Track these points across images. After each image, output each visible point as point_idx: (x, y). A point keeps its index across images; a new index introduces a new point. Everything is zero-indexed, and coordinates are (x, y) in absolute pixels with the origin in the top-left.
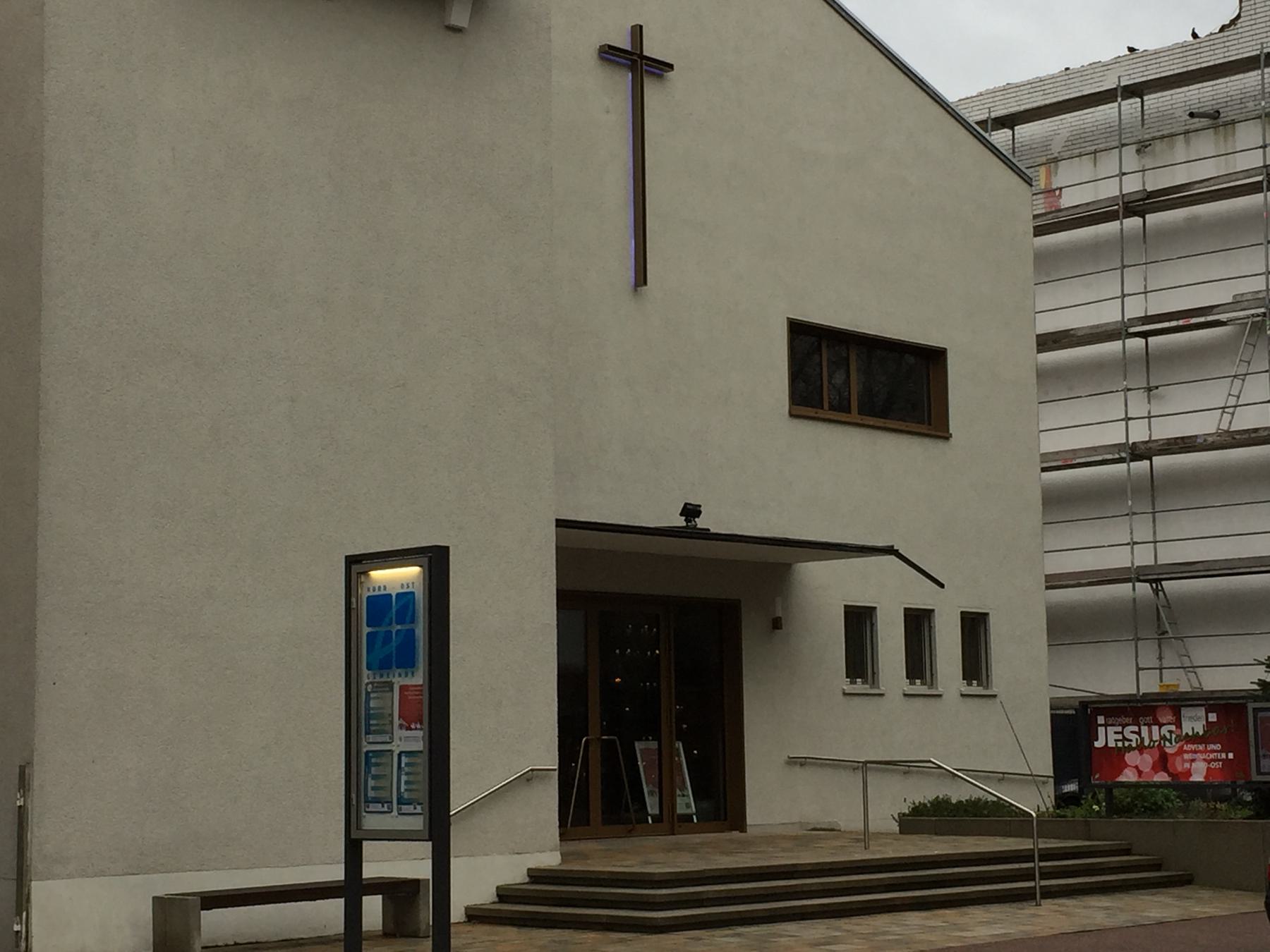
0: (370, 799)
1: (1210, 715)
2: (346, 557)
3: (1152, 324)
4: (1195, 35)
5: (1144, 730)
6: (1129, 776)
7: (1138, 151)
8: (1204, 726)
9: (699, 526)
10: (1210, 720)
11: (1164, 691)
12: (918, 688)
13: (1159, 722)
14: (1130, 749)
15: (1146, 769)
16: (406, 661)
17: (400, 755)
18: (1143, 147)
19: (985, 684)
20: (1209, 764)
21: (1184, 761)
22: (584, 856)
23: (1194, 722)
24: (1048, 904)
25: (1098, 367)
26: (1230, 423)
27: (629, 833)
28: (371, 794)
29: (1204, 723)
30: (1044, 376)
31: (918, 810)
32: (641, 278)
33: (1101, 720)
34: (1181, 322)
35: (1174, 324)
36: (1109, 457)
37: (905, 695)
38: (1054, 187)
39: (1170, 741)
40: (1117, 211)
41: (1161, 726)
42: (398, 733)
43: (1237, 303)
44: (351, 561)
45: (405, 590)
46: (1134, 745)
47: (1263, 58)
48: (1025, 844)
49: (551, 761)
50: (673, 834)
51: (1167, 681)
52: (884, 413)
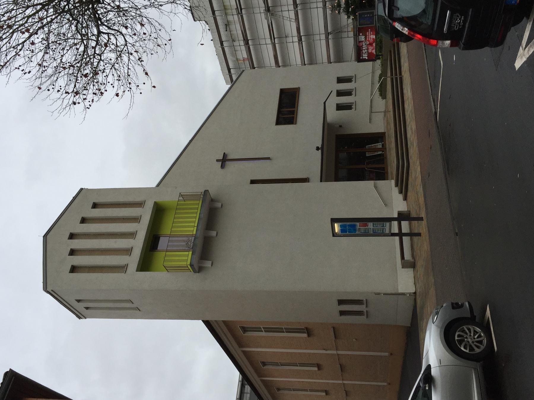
3: (272, 37)
4: (212, 40)
5: (363, 48)
6: (374, 51)
7: (234, 42)
9: (321, 147)
11: (353, 31)
12: (354, 93)
14: (368, 51)
15: (372, 48)
16: (354, 226)
17: (374, 227)
18: (234, 41)
19: (352, 77)
21: (371, 40)
22: (392, 174)
23: (362, 38)
24: (403, 74)
25: (282, 48)
26: (293, 19)
27: (386, 158)
28: (382, 232)
30: (285, 65)
31: (381, 95)
32: (268, 158)
33: (361, 58)
34: (271, 31)
35: (272, 33)
36: (301, 45)
37: (355, 96)
38: (243, 59)
39: (366, 43)
40: (248, 46)
41: (363, 45)
42: (369, 227)
43: (267, 18)
44: (334, 236)
46: (367, 51)
47: (214, 16)
48: (389, 80)
49: (372, 182)
50: (386, 148)
51: (351, 30)
52: (294, 105)
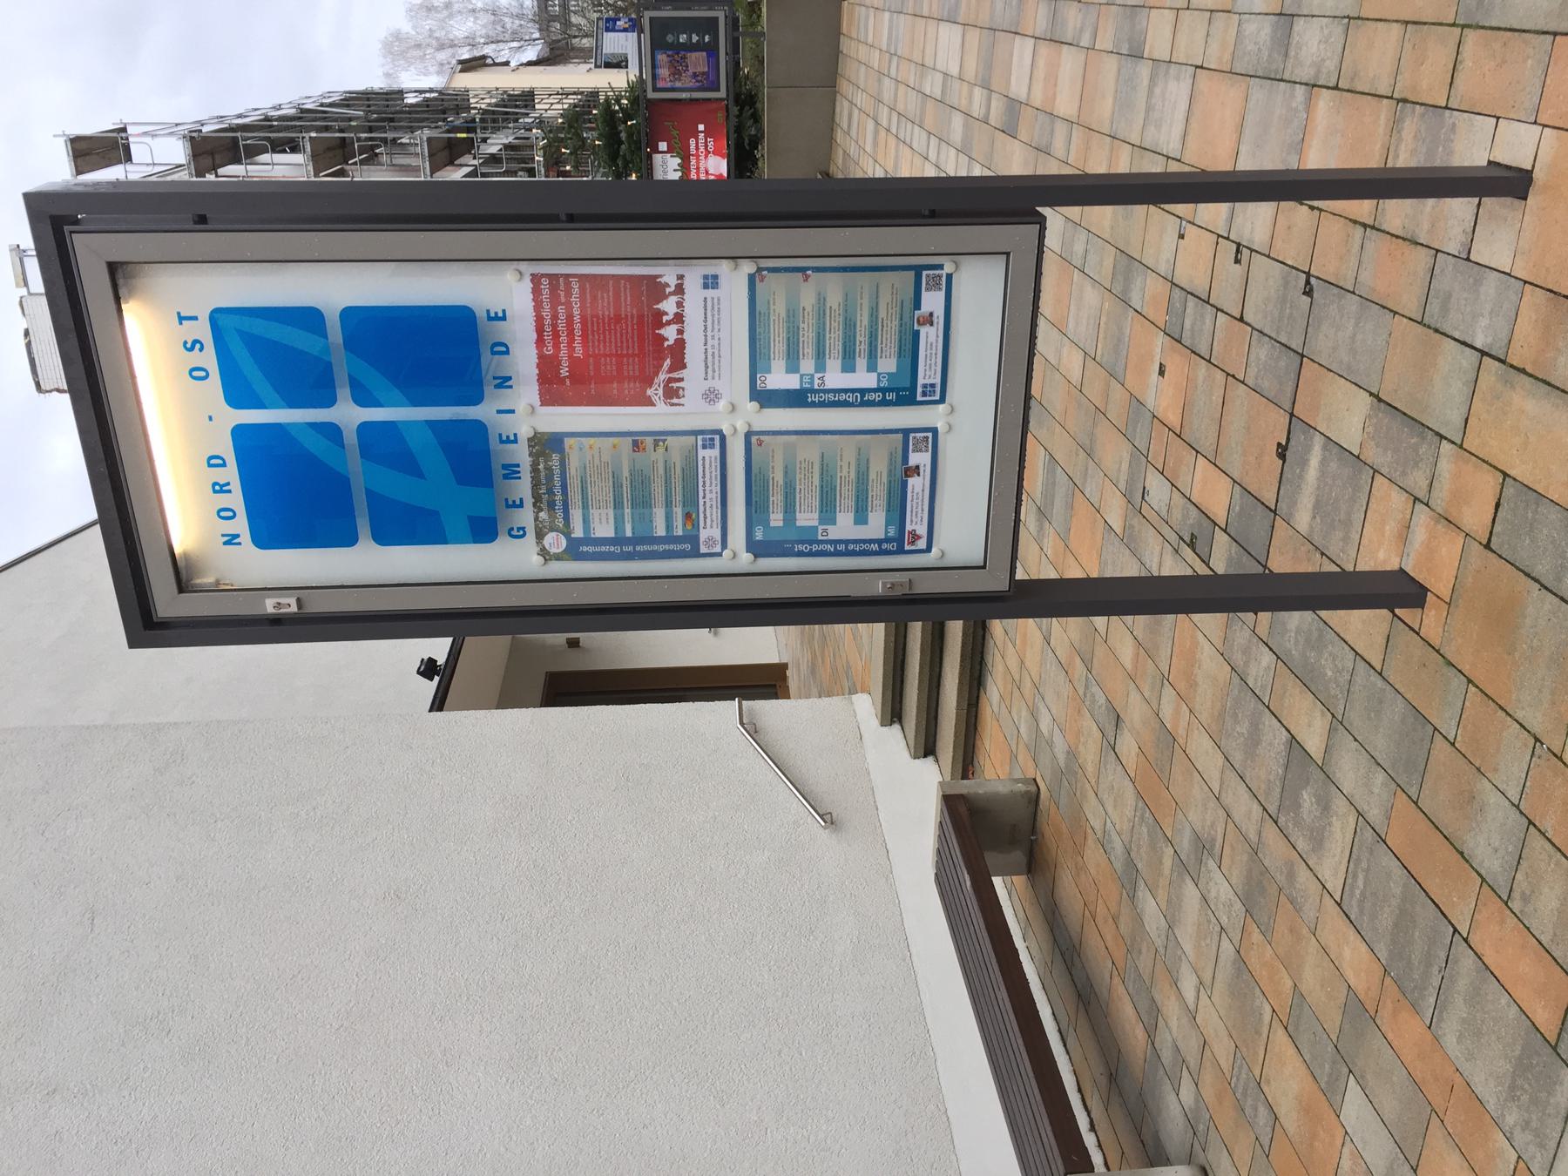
0: (892, 532)
1: (660, 149)
2: (134, 643)
8: (671, 156)
10: (666, 149)
13: (674, 323)
17: (765, 398)
20: (709, 152)
28: (876, 525)
29: (669, 155)
45: (209, 358)
